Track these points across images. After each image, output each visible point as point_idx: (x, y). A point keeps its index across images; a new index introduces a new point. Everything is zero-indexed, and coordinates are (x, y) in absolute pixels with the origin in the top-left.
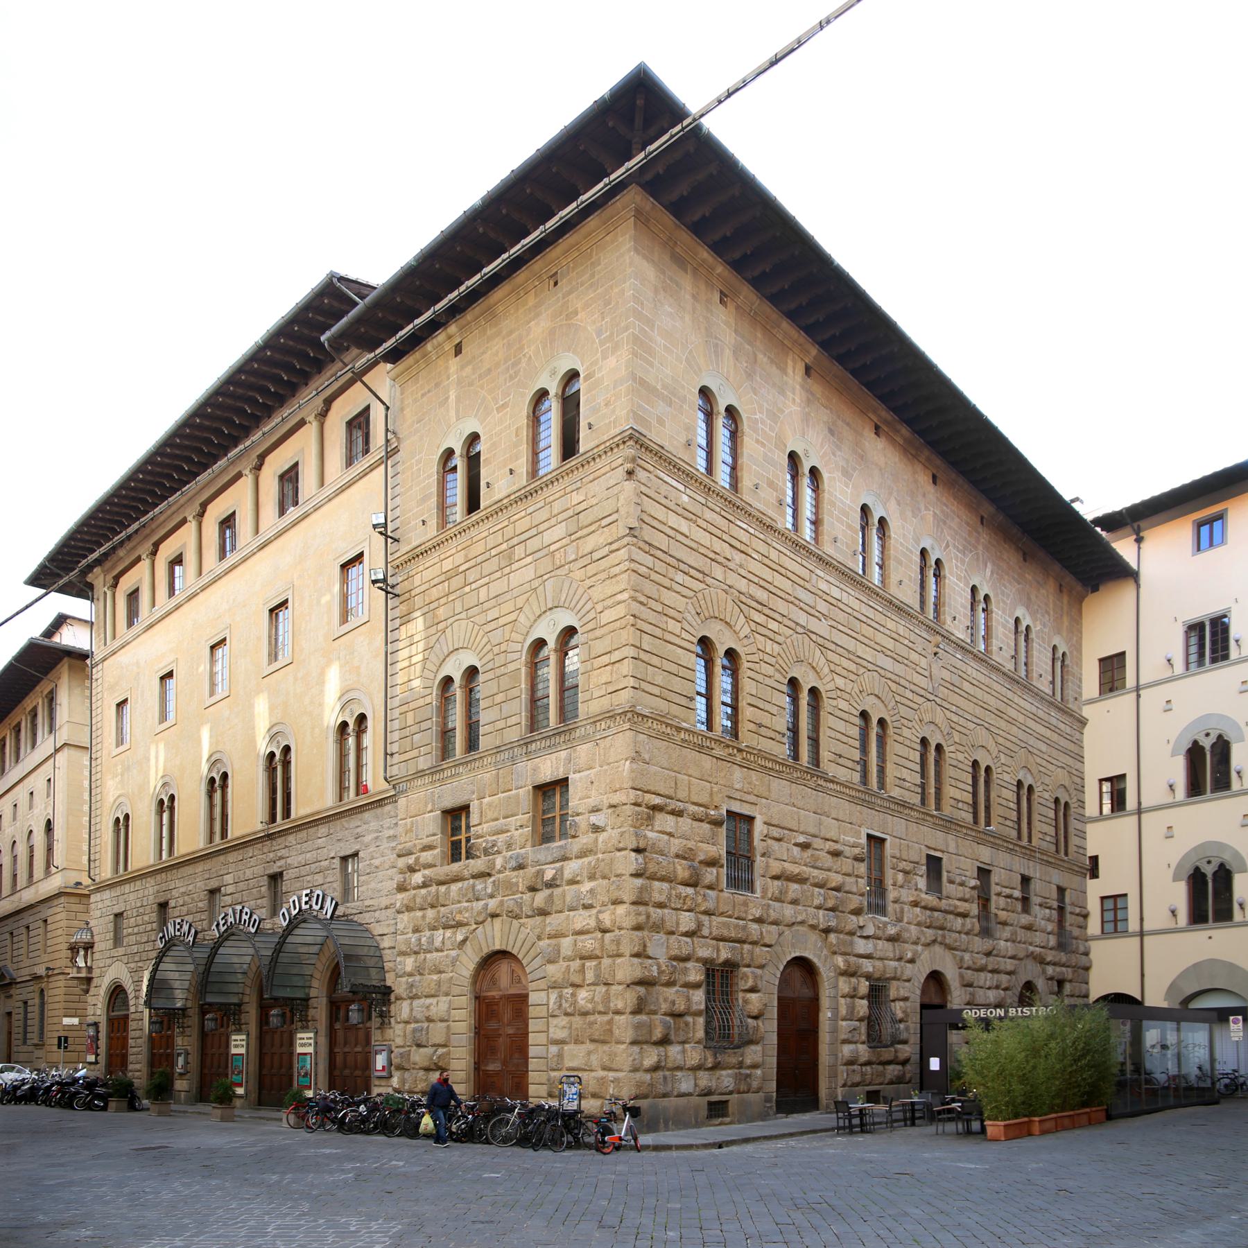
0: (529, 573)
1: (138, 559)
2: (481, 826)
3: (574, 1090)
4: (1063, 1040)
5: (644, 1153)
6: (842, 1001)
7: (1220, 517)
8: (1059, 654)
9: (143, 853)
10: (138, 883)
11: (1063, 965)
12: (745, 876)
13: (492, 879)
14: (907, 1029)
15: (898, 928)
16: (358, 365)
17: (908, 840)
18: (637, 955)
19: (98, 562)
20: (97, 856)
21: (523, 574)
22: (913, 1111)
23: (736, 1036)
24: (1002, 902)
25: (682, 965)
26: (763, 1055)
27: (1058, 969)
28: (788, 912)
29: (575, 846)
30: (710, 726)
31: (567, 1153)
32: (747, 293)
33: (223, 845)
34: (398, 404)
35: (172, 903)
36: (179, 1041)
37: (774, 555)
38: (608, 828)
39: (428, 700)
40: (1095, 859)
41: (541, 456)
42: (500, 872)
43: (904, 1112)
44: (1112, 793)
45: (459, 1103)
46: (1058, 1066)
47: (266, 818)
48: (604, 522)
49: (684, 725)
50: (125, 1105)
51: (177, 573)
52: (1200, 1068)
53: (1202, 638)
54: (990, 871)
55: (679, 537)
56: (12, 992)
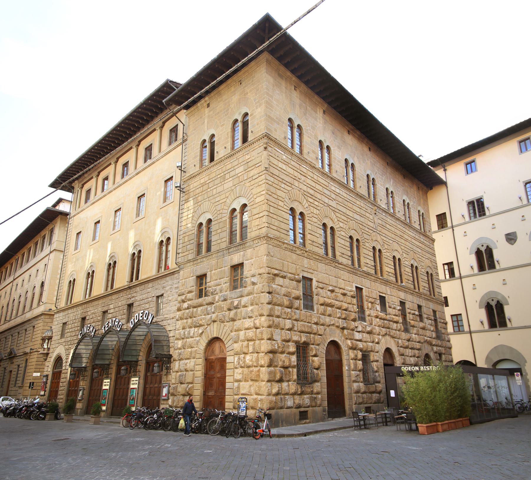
0: (231, 184)
1: (92, 178)
2: (210, 283)
3: (244, 405)
4: (445, 383)
5: (273, 439)
6: (351, 361)
7: (473, 161)
8: (421, 214)
9: (79, 296)
10: (75, 309)
11: (440, 346)
12: (310, 304)
13: (214, 305)
14: (379, 375)
15: (371, 328)
16: (175, 110)
17: (372, 289)
18: (269, 339)
19: (77, 179)
20: (60, 297)
21: (229, 184)
22: (386, 418)
23: (310, 378)
24: (411, 316)
25: (287, 344)
26: (321, 387)
27: (438, 348)
28: (328, 320)
29: (246, 291)
30: (295, 243)
31: (241, 439)
32: (303, 86)
33: (112, 292)
34: (187, 124)
35: (87, 318)
37: (315, 177)
38: (258, 283)
39: (193, 232)
40: (446, 298)
41: (236, 142)
42: (217, 302)
43: (382, 419)
44: (449, 269)
45: (196, 412)
46: (445, 396)
47: (129, 280)
48: (257, 166)
50: (53, 416)
51: (105, 184)
52: (506, 398)
53: (474, 207)
54: (405, 303)
55: (283, 171)
56: (14, 360)
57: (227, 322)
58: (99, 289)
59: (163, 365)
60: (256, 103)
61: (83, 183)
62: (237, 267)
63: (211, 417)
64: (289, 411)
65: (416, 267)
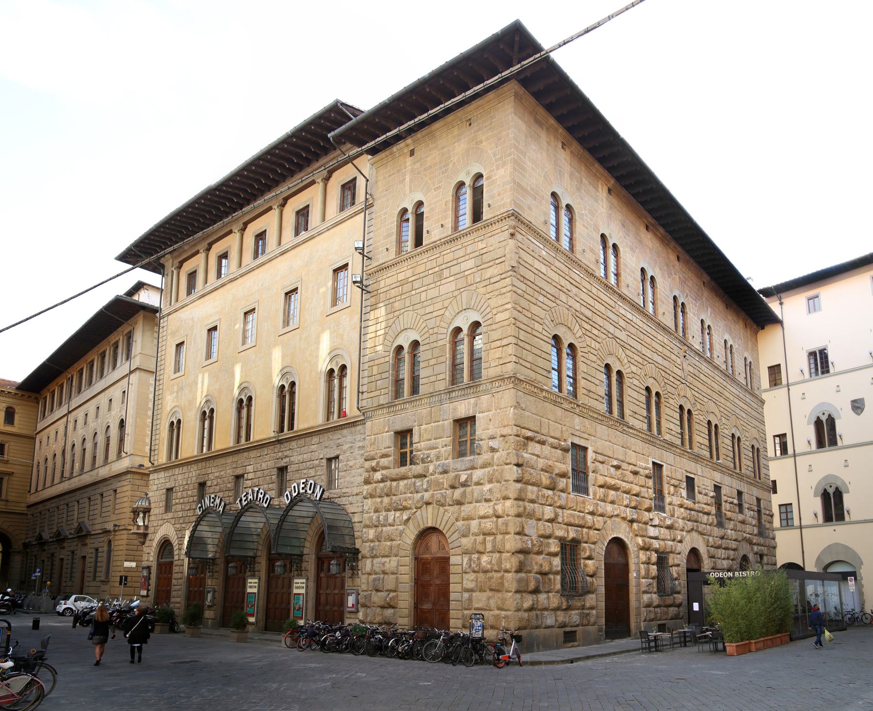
0: (452, 287)
1: (197, 252)
2: (420, 444)
3: (479, 623)
5: (524, 667)
6: (642, 566)
8: (748, 363)
10: (185, 468)
11: (762, 545)
14: (680, 584)
17: (676, 467)
18: (518, 533)
21: (448, 287)
22: (685, 637)
24: (728, 506)
25: (546, 541)
26: (597, 600)
27: (760, 548)
28: (609, 508)
30: (560, 390)
31: (475, 668)
32: (576, 145)
34: (374, 179)
35: (209, 483)
36: (209, 582)
37: (594, 291)
38: (500, 450)
39: (387, 359)
40: (774, 482)
41: (460, 219)
42: (432, 475)
48: (497, 261)
49: (545, 387)
50: (167, 628)
51: (223, 264)
53: (816, 360)
55: (541, 275)
57: (450, 505)
58: (224, 439)
59: (345, 563)
60: (496, 160)
61: (180, 259)
62: (465, 423)
63: (430, 634)
64: (548, 631)
65: (739, 438)
